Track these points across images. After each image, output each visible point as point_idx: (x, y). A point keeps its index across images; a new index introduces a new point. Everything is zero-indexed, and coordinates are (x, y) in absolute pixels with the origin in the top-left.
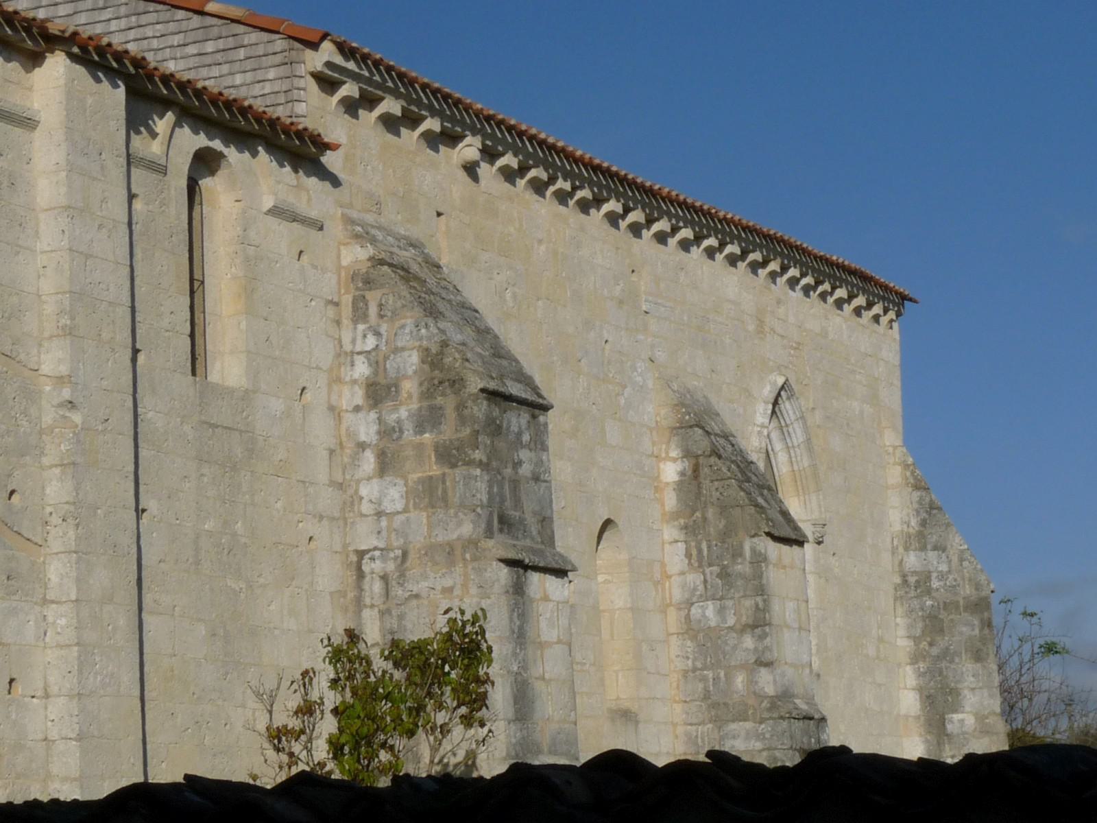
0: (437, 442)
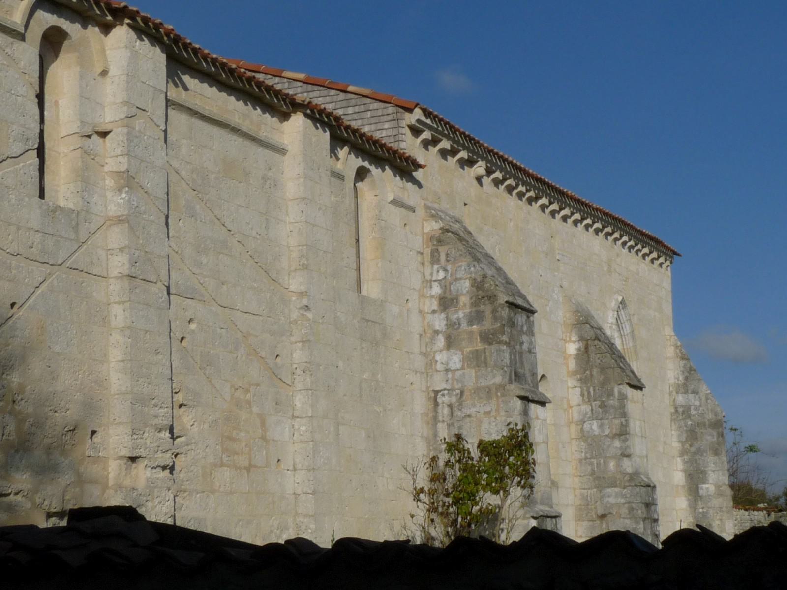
0: (481, 331)
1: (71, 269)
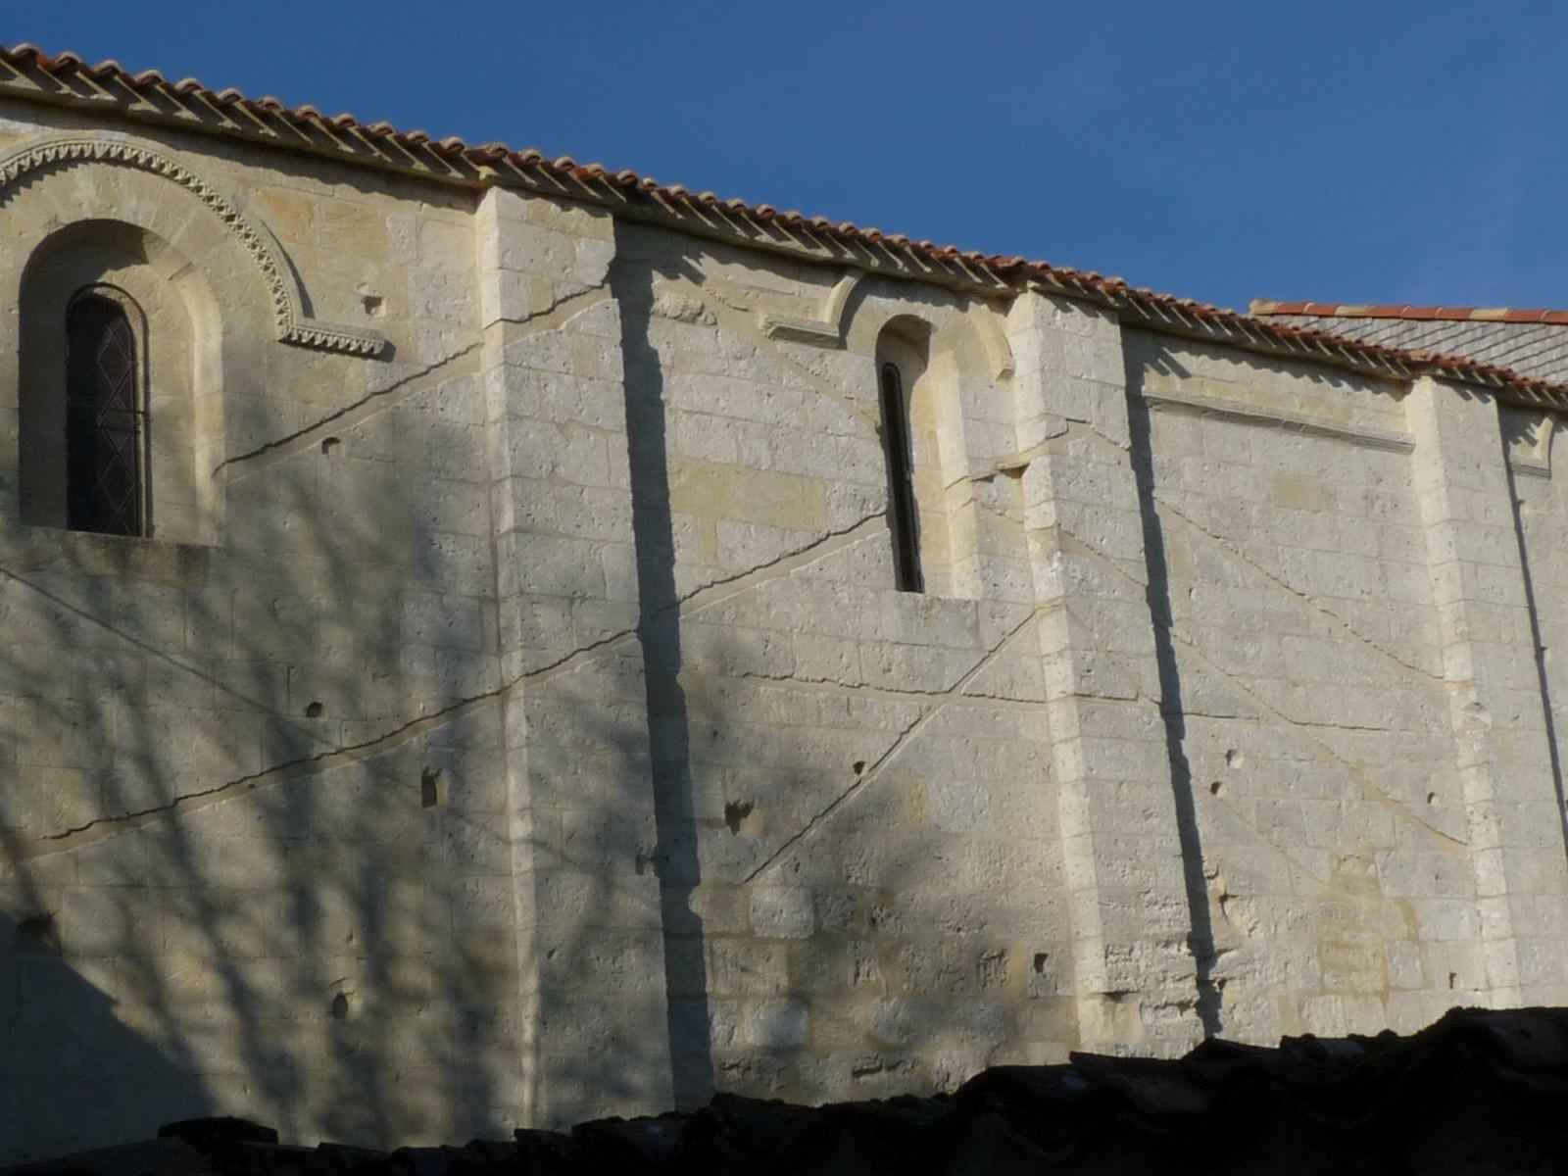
1: (970, 695)
